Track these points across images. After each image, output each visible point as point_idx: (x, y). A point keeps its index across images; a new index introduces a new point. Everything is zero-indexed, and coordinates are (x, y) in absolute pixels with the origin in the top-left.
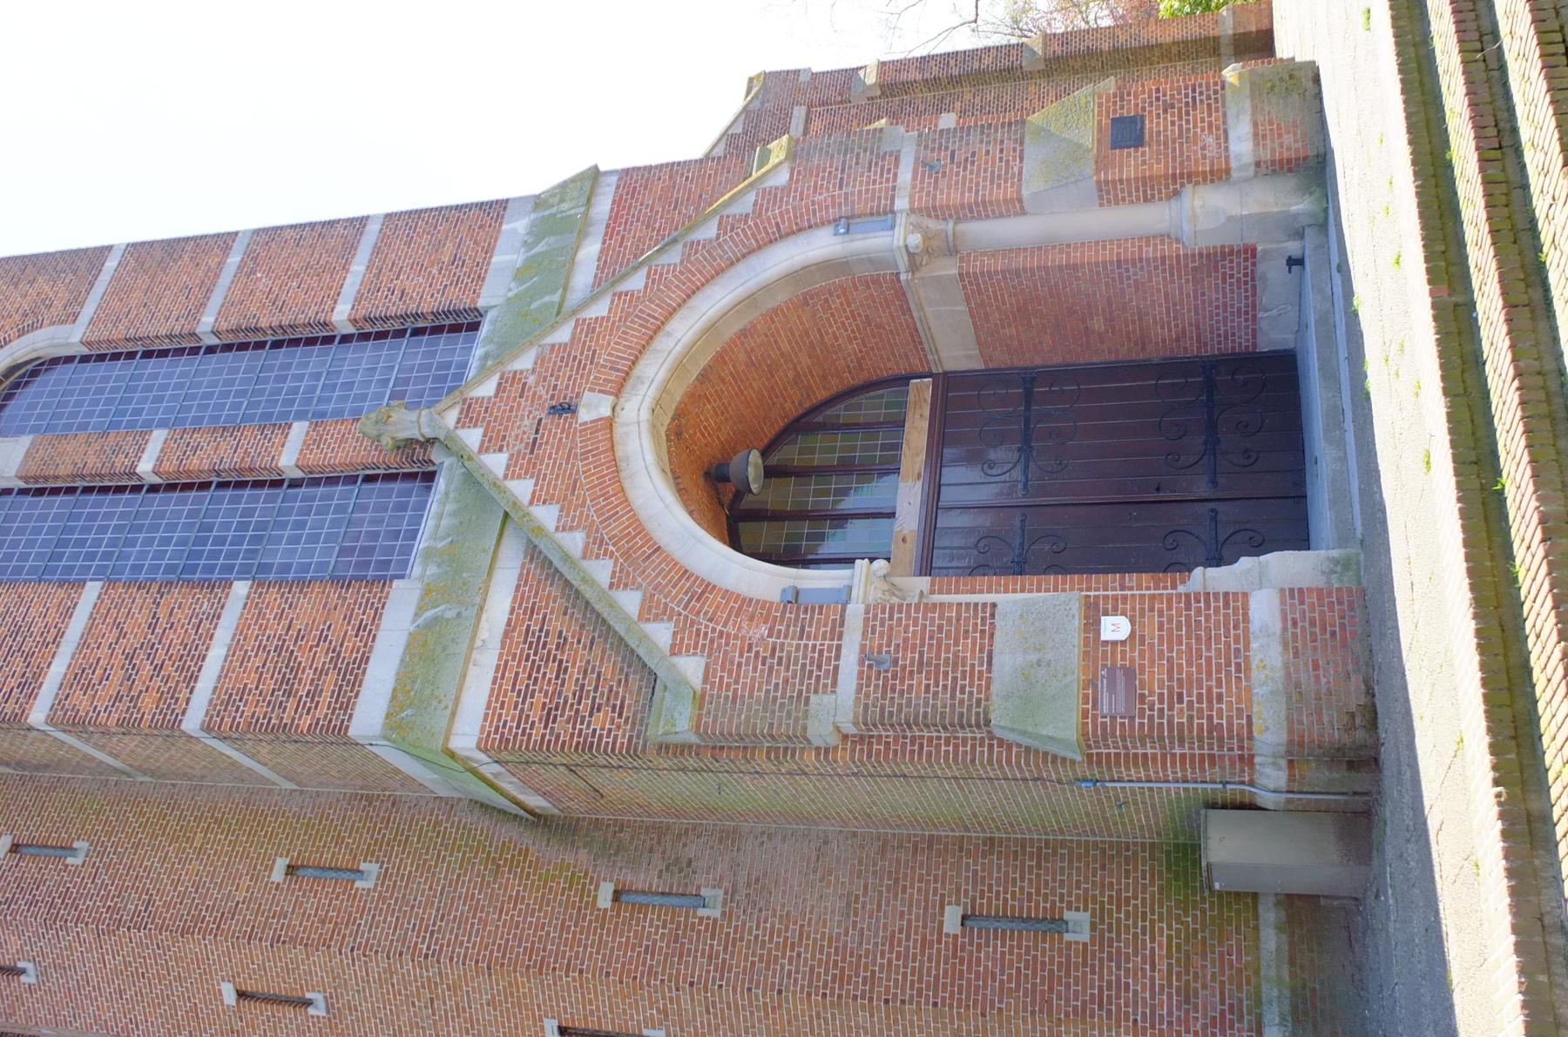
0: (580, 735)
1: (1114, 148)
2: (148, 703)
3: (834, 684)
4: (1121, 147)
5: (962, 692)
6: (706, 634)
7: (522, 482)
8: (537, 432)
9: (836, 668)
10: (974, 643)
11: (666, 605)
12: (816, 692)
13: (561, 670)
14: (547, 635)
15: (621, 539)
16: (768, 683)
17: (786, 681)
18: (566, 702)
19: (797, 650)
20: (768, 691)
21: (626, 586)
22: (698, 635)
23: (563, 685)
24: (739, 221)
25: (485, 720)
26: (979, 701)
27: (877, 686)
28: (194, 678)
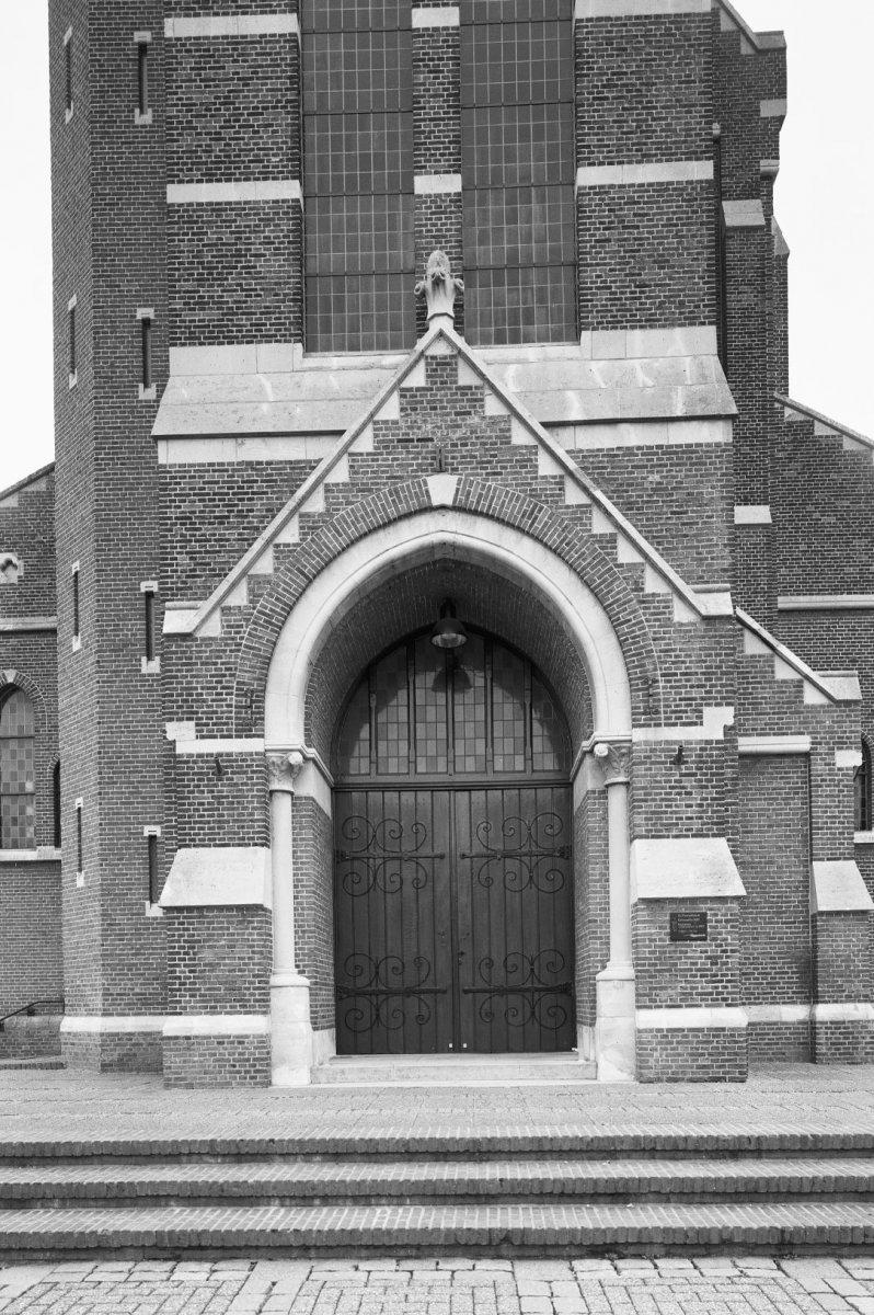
0: (172, 548)
1: (672, 915)
2: (188, 140)
3: (203, 737)
4: (672, 920)
5: (200, 829)
6: (238, 633)
7: (371, 440)
8: (418, 440)
9: (215, 737)
10: (235, 833)
11: (261, 595)
12: (197, 725)
13: (222, 519)
14: (249, 499)
15: (317, 545)
16: (202, 688)
17: (204, 701)
18: (197, 529)
19: (228, 706)
20: (196, 688)
21: (277, 558)
22: (238, 626)
23: (210, 523)
24: (636, 583)
25: (180, 466)
26: (194, 840)
27: (202, 768)
28: (210, 177)
